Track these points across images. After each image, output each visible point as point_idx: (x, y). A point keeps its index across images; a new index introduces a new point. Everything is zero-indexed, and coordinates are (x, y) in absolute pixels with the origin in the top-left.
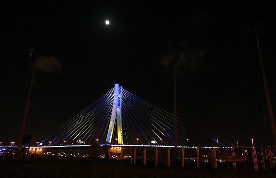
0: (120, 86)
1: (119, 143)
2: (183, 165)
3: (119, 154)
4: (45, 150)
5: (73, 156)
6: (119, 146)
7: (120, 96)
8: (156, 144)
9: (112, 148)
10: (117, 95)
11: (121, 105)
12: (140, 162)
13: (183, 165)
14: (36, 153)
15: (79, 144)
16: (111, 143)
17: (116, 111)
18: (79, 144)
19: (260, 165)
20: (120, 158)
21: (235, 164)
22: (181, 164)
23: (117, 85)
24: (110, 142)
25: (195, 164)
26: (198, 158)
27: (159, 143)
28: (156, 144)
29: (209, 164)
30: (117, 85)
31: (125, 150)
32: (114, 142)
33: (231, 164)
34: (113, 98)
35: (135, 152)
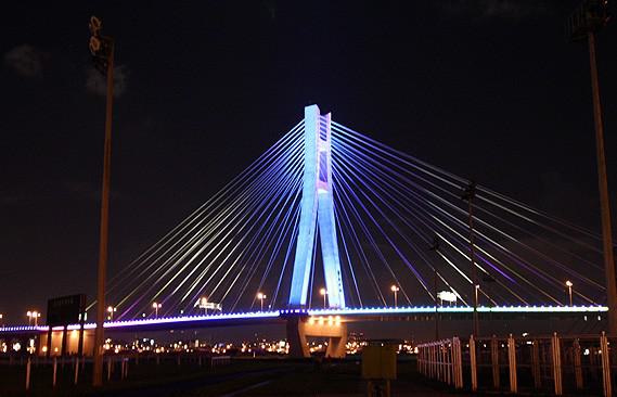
1: (331, 303)
3: (336, 340)
5: (112, 350)
6: (334, 316)
7: (326, 147)
8: (459, 303)
9: (311, 321)
11: (329, 136)
15: (202, 312)
17: (317, 198)
18: (202, 312)
19: (568, 377)
23: (312, 111)
24: (303, 301)
26: (575, 336)
27: (467, 296)
30: (312, 111)
31: (354, 327)
32: (317, 301)
35: (421, 162)
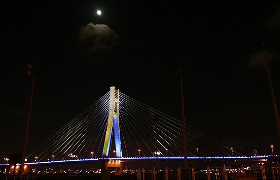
3: (118, 169)
7: (117, 101)
9: (110, 162)
24: (107, 155)
30: (113, 88)
31: (125, 164)
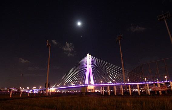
0: (90, 55)
2: (131, 94)
3: (93, 90)
4: (56, 90)
8: (112, 83)
10: (89, 60)
12: (106, 93)
13: (131, 94)
14: (52, 92)
15: (72, 86)
16: (88, 84)
20: (93, 92)
21: (160, 92)
22: (129, 94)
25: (137, 92)
28: (112, 83)
29: (145, 92)
30: (88, 55)
31: (96, 88)
32: (89, 84)
33: (158, 92)
34: (86, 63)
35: (103, 88)
